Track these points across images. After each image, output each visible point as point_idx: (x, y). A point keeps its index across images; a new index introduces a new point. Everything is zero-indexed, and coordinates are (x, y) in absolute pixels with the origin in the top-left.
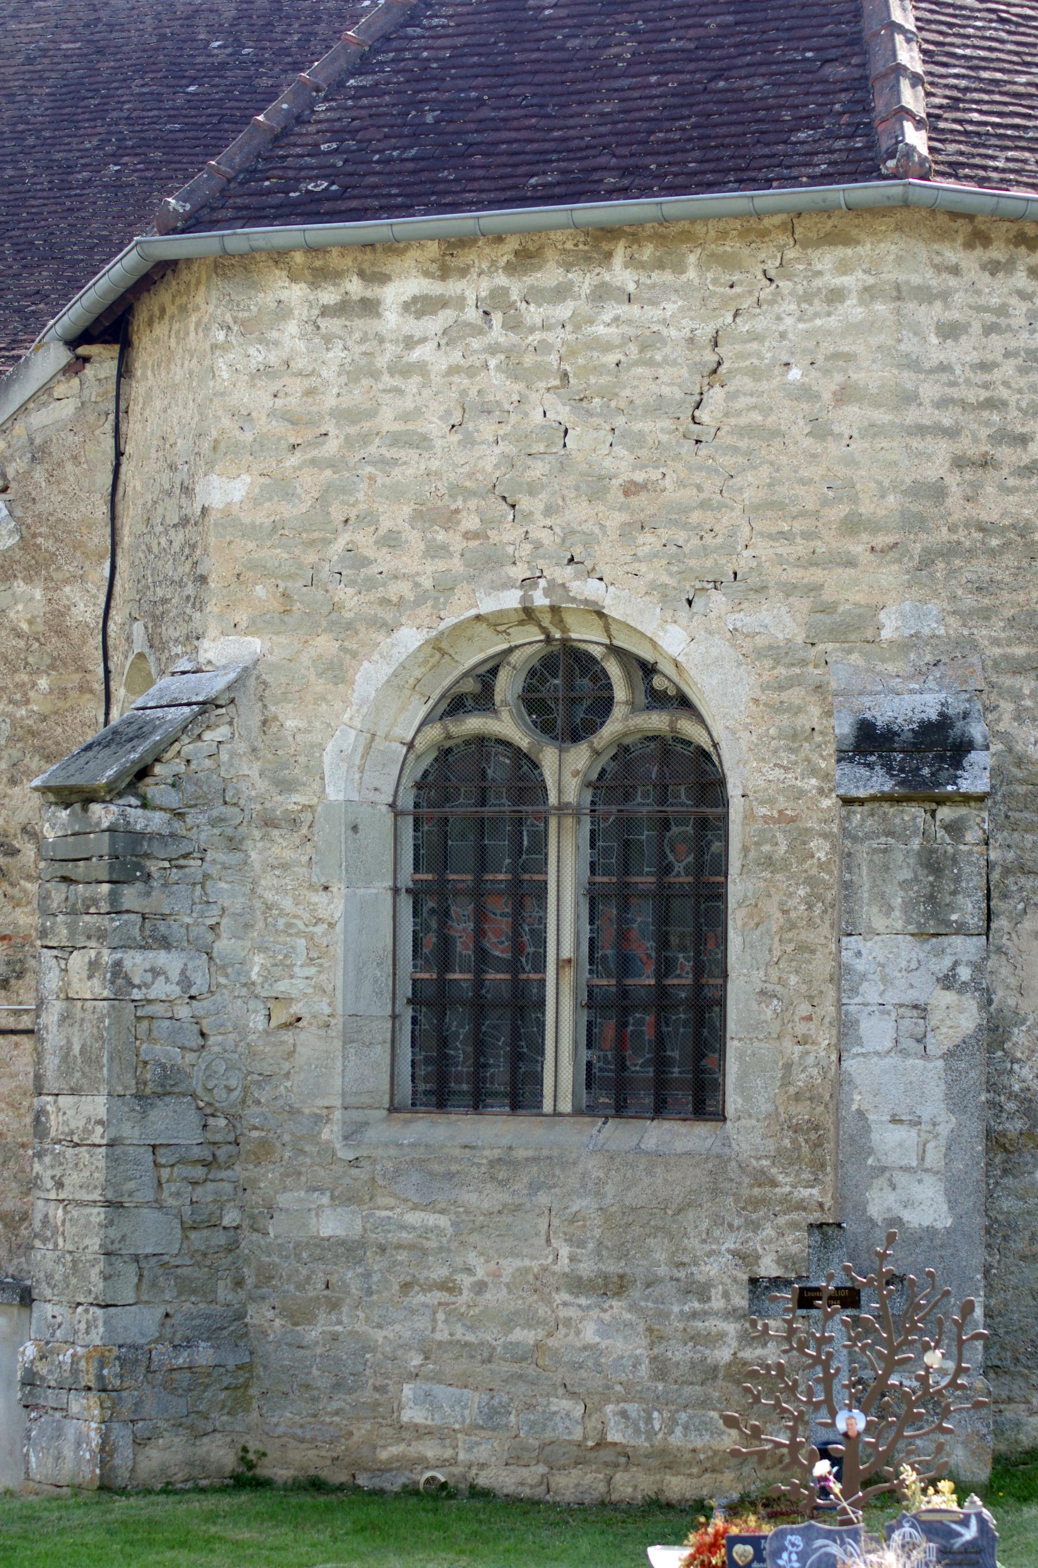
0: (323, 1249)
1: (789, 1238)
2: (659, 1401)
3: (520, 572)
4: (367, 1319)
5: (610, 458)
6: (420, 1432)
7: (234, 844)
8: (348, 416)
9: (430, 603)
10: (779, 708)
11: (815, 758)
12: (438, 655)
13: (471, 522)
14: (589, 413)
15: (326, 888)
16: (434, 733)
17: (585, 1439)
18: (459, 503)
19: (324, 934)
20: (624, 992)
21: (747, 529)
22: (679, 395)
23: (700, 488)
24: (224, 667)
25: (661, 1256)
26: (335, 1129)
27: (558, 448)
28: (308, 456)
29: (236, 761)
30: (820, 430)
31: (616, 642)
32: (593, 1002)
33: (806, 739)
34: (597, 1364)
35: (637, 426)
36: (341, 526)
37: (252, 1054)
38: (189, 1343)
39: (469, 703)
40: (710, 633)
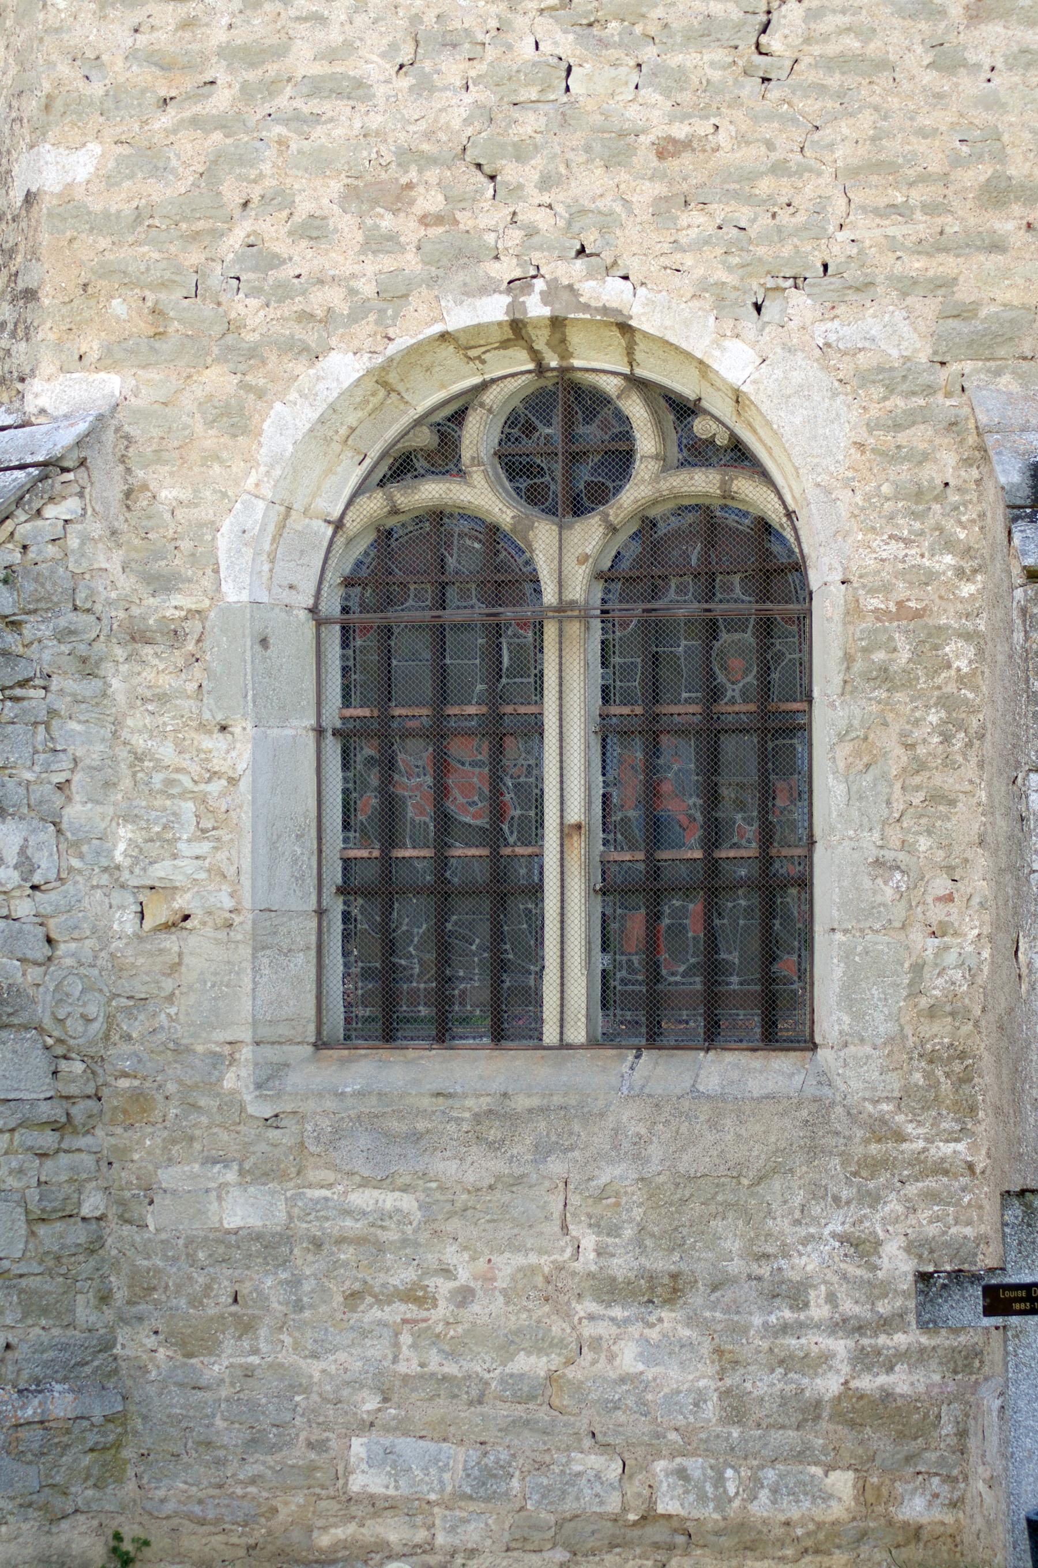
0: (229, 1246)
1: (924, 1216)
2: (736, 1455)
3: (506, 269)
4: (297, 1346)
5: (635, 106)
6: (377, 1506)
7: (88, 667)
8: (240, 56)
9: (372, 317)
10: (892, 457)
11: (949, 524)
12: (382, 393)
13: (430, 201)
14: (604, 44)
15: (224, 728)
16: (373, 505)
17: (625, 1510)
18: (413, 175)
19: (222, 795)
20: (655, 870)
21: (843, 201)
22: (736, 14)
23: (770, 145)
24: (66, 417)
25: (733, 1245)
26: (243, 1073)
27: (558, 94)
28: (187, 114)
29: (89, 548)
30: (947, 59)
31: (639, 372)
32: (610, 887)
33: (936, 499)
34: (642, 1402)
35: (675, 60)
36: (237, 213)
37: (119, 969)
38: (38, 1387)
39: (421, 464)
40: (791, 350)
